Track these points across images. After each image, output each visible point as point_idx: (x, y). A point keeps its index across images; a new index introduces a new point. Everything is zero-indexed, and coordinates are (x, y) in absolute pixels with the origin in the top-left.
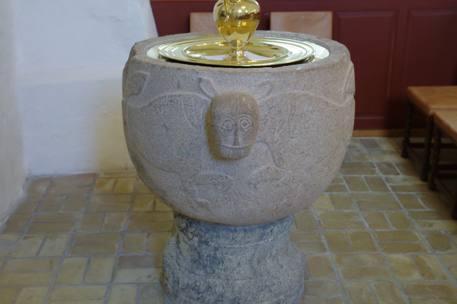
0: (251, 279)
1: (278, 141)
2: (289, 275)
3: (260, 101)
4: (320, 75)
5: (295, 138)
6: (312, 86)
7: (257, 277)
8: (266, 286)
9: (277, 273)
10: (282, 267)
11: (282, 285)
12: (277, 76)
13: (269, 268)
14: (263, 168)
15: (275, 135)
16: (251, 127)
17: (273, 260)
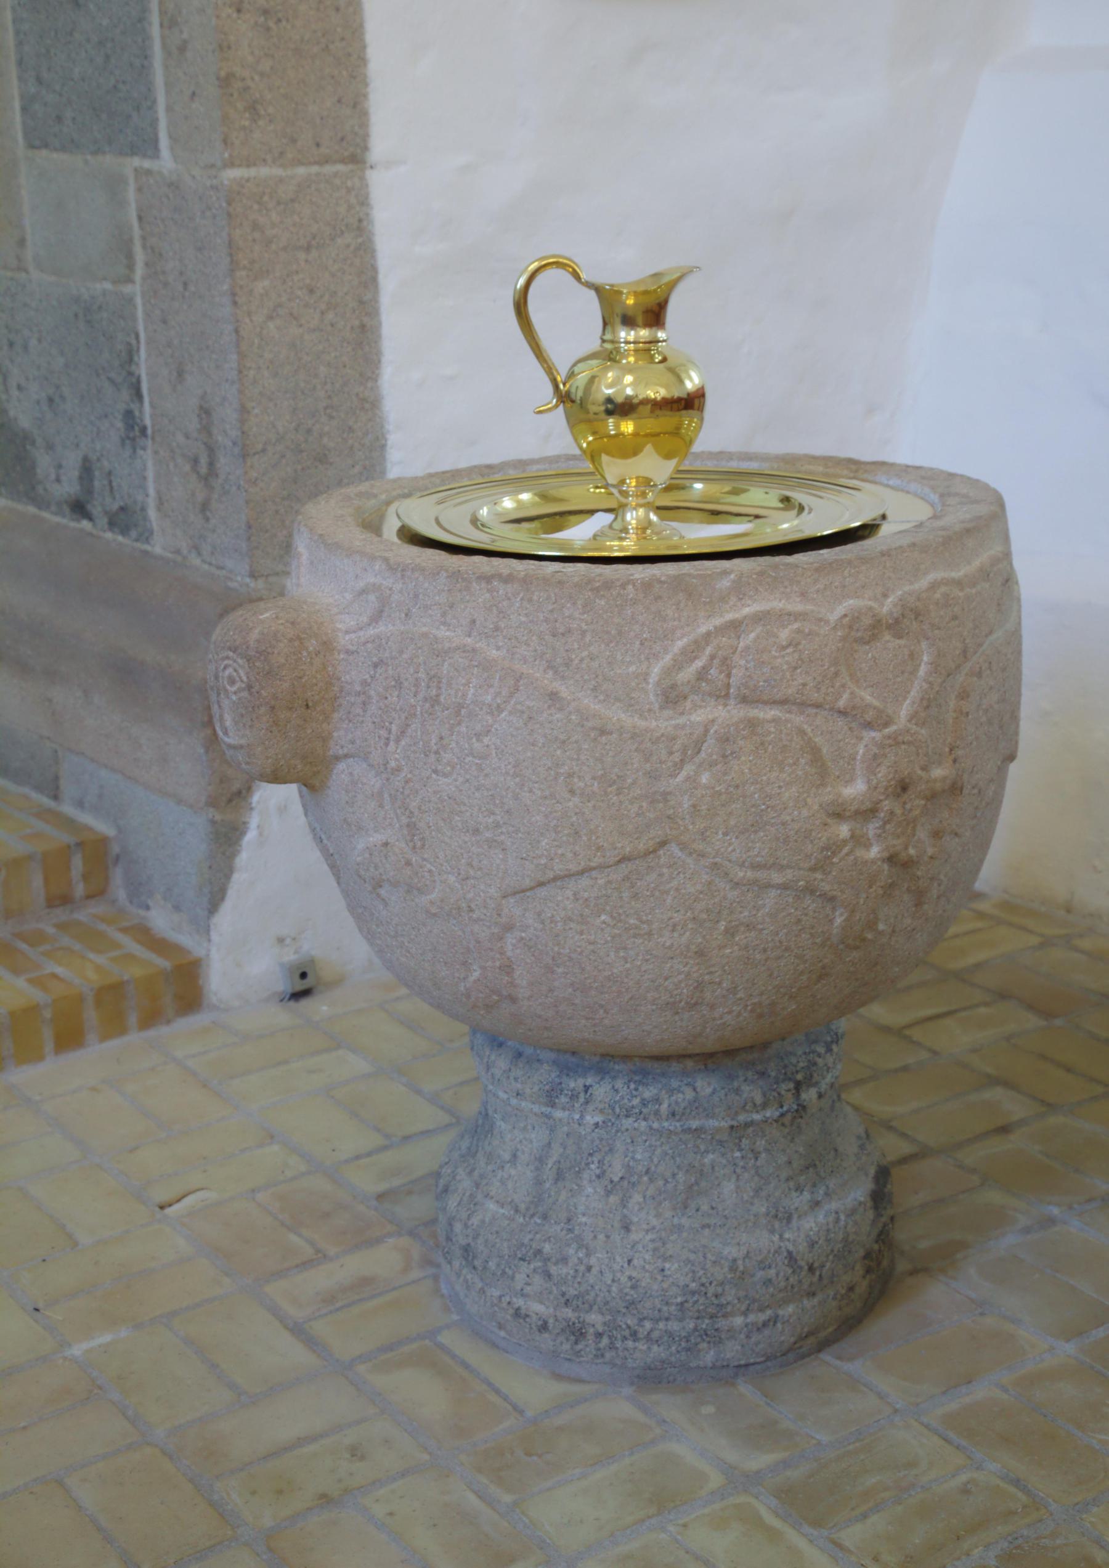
0: (517, 1211)
1: (398, 769)
2: (635, 1262)
3: (353, 636)
4: (530, 600)
5: (445, 775)
6: (497, 629)
7: (533, 1216)
8: (539, 1252)
9: (601, 1237)
10: (627, 1229)
11: (591, 1278)
12: (399, 575)
13: (581, 1208)
14: (377, 838)
15: (389, 748)
16: (245, 694)
17: (608, 1193)
